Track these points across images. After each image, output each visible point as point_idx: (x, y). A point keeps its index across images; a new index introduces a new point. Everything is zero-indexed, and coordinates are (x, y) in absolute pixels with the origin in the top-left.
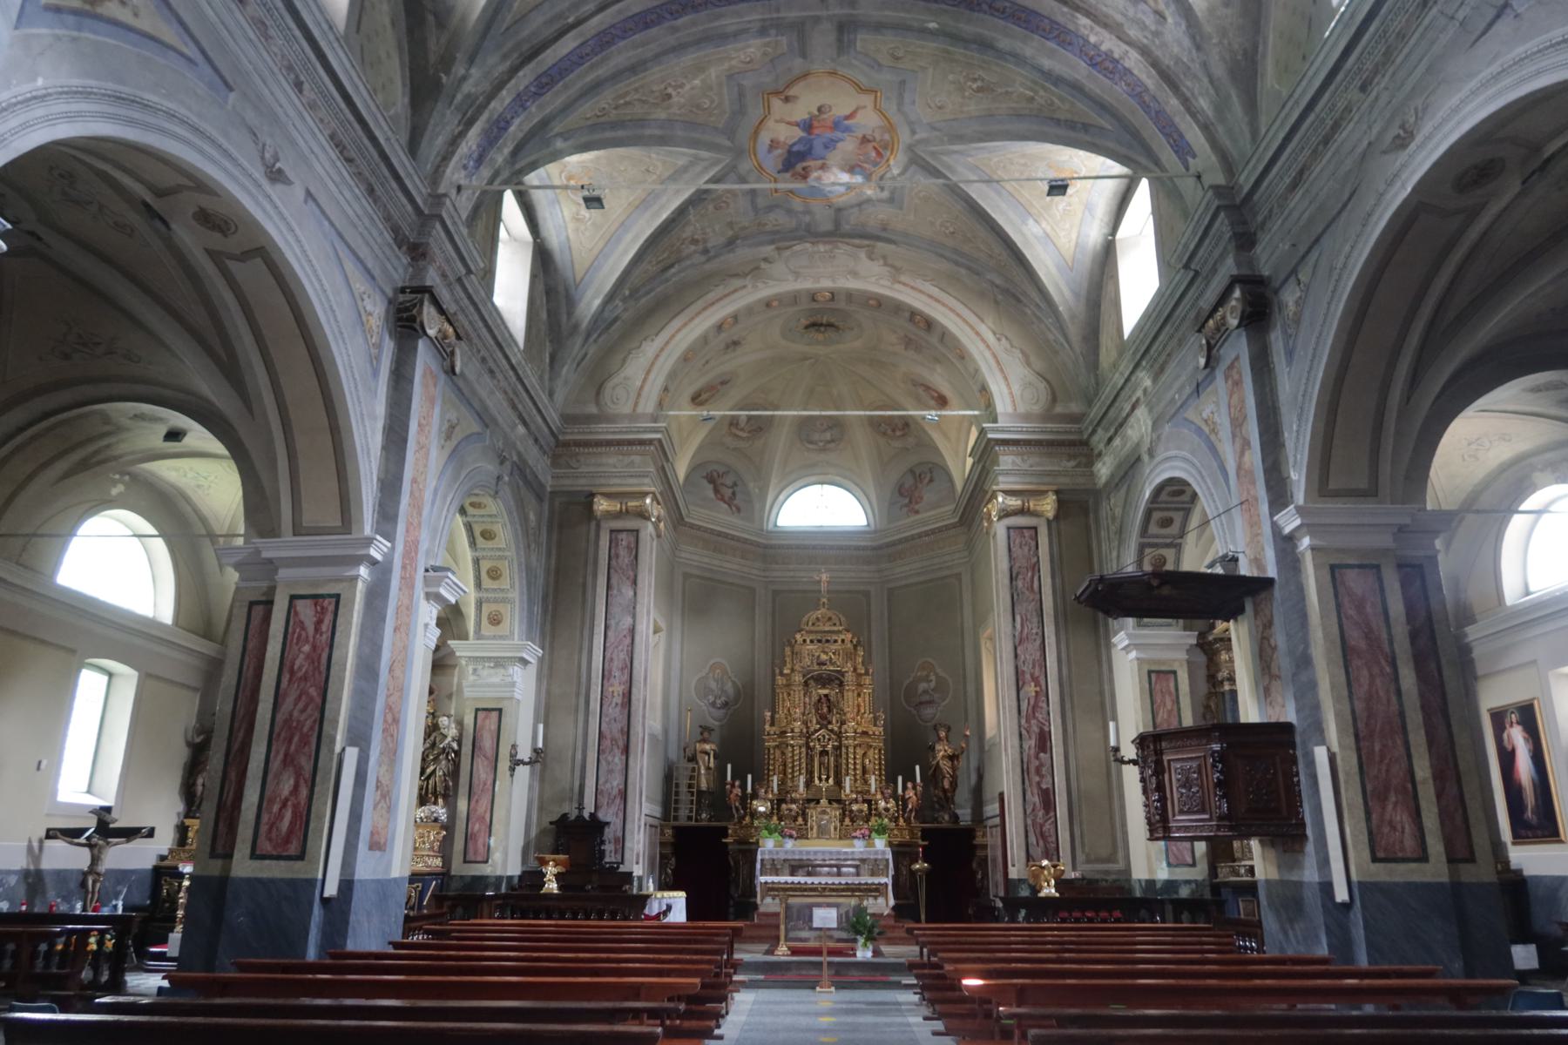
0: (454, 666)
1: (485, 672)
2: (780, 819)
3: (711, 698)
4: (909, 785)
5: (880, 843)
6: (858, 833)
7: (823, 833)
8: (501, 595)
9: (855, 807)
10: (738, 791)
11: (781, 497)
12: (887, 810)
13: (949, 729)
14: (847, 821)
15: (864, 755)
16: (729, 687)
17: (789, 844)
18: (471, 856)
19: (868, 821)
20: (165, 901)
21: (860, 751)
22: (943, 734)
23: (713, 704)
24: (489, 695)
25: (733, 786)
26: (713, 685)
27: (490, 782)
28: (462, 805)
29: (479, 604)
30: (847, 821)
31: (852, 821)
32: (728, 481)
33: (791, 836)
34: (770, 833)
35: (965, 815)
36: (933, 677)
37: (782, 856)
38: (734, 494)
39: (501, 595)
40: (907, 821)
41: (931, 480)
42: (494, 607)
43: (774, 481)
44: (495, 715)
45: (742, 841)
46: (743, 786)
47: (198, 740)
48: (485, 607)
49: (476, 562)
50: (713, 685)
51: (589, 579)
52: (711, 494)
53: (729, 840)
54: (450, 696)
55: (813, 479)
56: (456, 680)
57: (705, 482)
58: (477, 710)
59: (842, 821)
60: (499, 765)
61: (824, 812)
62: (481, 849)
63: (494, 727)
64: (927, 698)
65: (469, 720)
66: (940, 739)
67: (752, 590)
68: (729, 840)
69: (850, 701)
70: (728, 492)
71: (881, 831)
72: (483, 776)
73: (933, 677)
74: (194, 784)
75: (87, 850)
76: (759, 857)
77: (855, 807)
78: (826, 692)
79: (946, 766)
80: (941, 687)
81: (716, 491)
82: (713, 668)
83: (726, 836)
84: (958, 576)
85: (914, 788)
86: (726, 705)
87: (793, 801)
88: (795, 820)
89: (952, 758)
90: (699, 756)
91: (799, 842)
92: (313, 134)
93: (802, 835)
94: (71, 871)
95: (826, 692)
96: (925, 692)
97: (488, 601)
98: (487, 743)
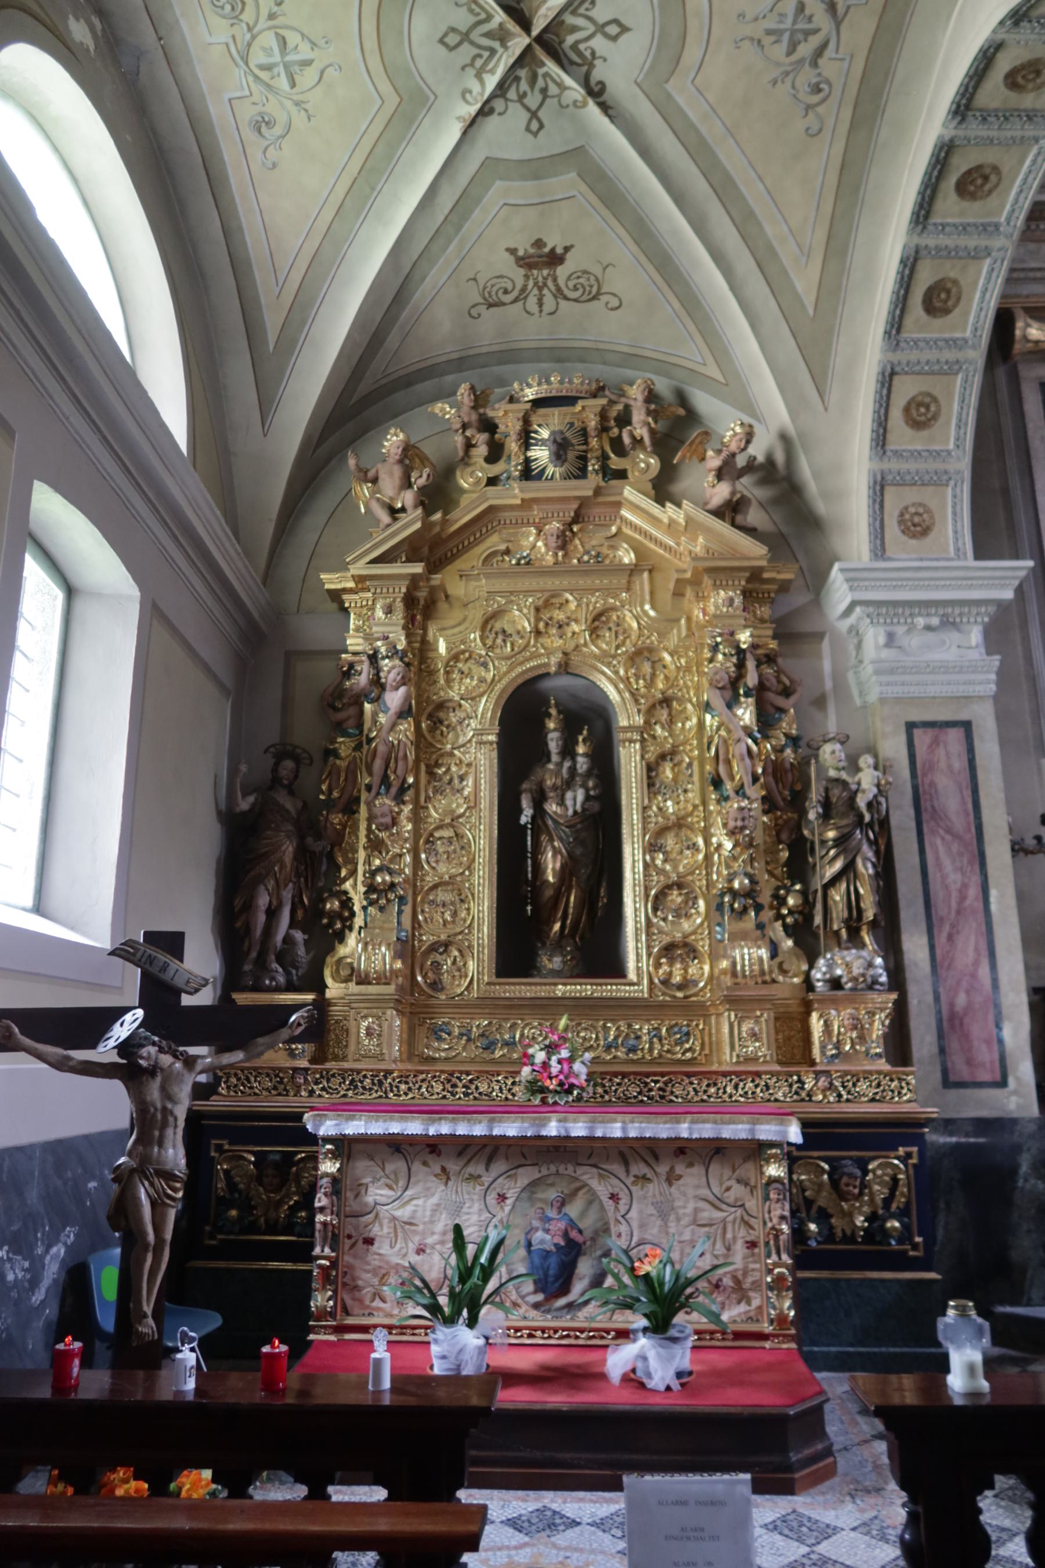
0: (820, 636)
1: (914, 641)
8: (932, 465)
18: (961, 1070)
20: (225, 1203)
24: (932, 691)
27: (973, 892)
28: (915, 947)
29: (879, 487)
39: (932, 465)
42: (911, 496)
44: (954, 735)
47: (245, 804)
48: (890, 494)
49: (888, 379)
51: (1015, 483)
54: (820, 702)
56: (827, 665)
58: (911, 727)
60: (990, 851)
62: (986, 1055)
63: (959, 764)
65: (894, 747)
72: (954, 879)
74: (249, 906)
75: (116, 1088)
94: (32, 1147)
97: (903, 482)
98: (951, 800)
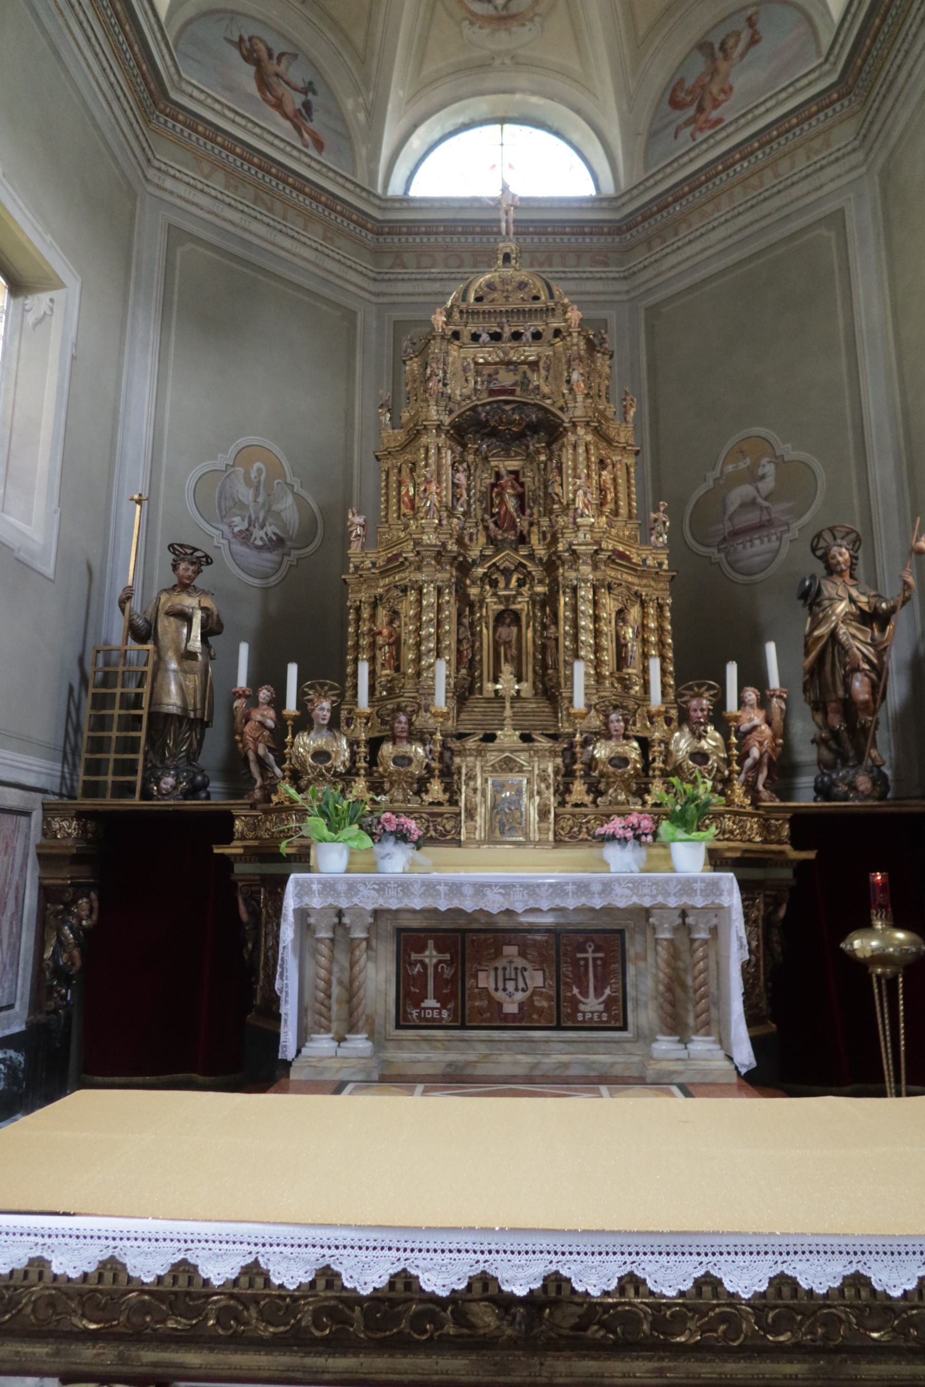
2: (376, 787)
3: (240, 524)
4: (751, 695)
5: (688, 856)
6: (616, 825)
7: (504, 825)
9: (601, 751)
10: (267, 716)
11: (416, 143)
12: (700, 757)
13: (856, 543)
14: (579, 787)
15: (621, 614)
16: (287, 506)
17: (397, 860)
19: (642, 791)
21: (610, 605)
22: (842, 555)
23: (245, 537)
25: (253, 701)
26: (245, 494)
30: (579, 787)
31: (595, 790)
32: (297, 74)
33: (402, 836)
34: (334, 827)
35: (258, 877)
36: (769, 469)
37: (369, 901)
38: (307, 105)
40: (751, 788)
41: (754, 41)
43: (397, 95)
45: (266, 853)
46: (278, 702)
50: (245, 494)
52: (252, 87)
53: (234, 849)
55: (481, 106)
57: (235, 55)
59: (563, 791)
61: (508, 765)
64: (752, 517)
66: (832, 570)
67: (350, 316)
68: (234, 849)
69: (577, 489)
70: (295, 100)
71: (689, 819)
73: (769, 469)
76: (290, 903)
77: (601, 751)
78: (513, 464)
79: (858, 641)
80: (795, 483)
81: (263, 83)
82: (245, 455)
83: (228, 838)
84: (837, 220)
85: (763, 703)
86: (278, 543)
87: (419, 736)
88: (421, 786)
89: (873, 618)
90: (166, 625)
91: (431, 853)
92: (15, 201)
93: (440, 833)
95: (513, 464)
96: (750, 504)
